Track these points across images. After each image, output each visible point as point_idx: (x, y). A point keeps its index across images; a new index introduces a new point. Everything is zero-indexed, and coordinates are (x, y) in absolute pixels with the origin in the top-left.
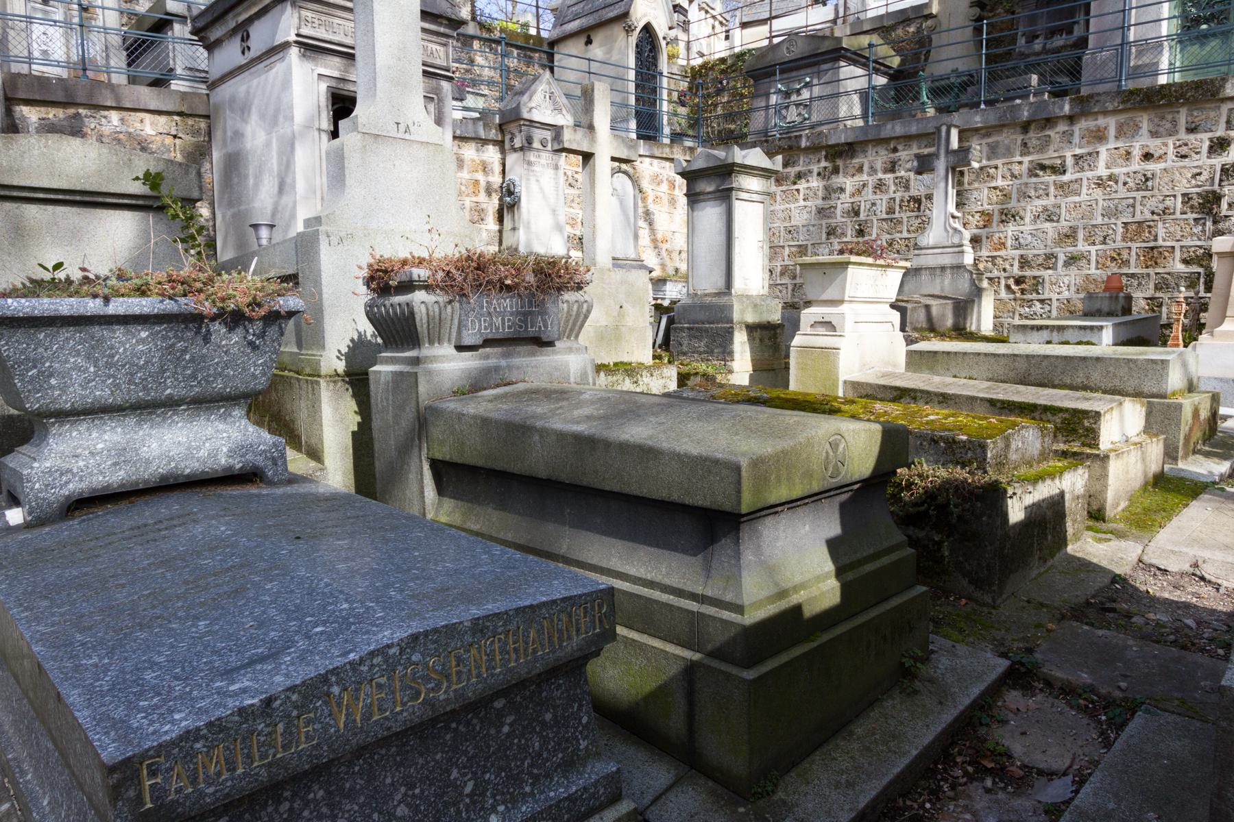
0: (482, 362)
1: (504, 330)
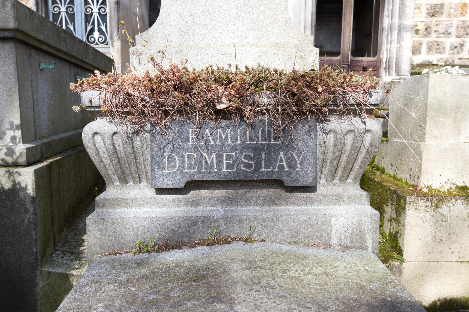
0: (187, 209)
1: (220, 170)
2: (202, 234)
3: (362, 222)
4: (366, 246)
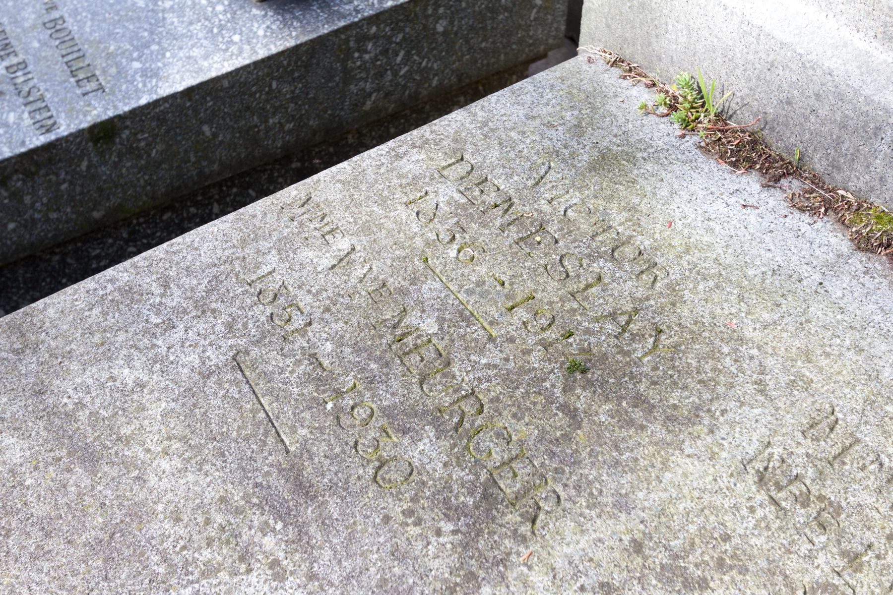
2: (877, 183)
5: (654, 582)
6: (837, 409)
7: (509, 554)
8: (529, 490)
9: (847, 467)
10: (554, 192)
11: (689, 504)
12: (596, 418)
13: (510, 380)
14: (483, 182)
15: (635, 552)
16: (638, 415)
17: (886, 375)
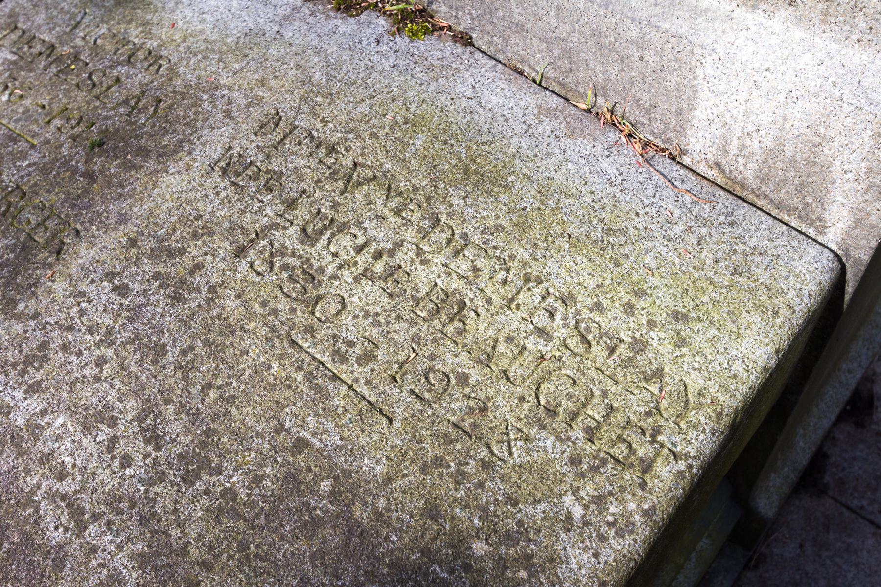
3: (831, 133)
4: (820, 219)
5: (146, 261)
6: (280, 110)
7: (38, 279)
8: (56, 235)
9: (287, 146)
10: (87, 30)
11: (170, 204)
12: (107, 173)
13: (44, 170)
14: (32, 39)
15: (131, 246)
16: (138, 160)
17: (317, 77)
